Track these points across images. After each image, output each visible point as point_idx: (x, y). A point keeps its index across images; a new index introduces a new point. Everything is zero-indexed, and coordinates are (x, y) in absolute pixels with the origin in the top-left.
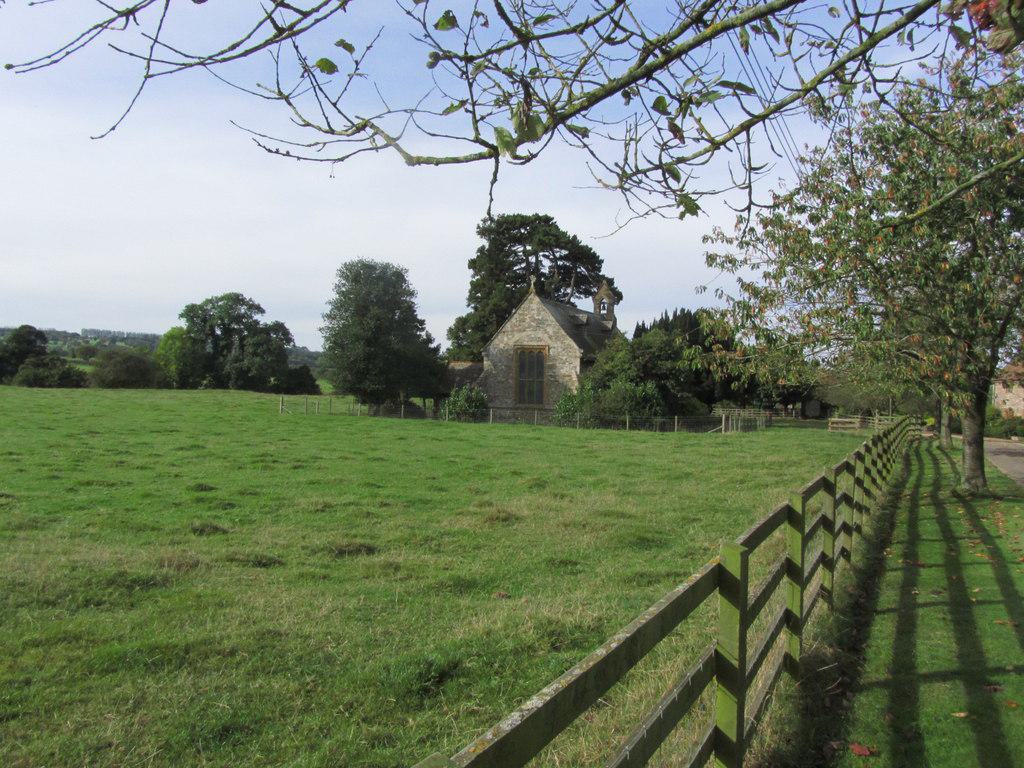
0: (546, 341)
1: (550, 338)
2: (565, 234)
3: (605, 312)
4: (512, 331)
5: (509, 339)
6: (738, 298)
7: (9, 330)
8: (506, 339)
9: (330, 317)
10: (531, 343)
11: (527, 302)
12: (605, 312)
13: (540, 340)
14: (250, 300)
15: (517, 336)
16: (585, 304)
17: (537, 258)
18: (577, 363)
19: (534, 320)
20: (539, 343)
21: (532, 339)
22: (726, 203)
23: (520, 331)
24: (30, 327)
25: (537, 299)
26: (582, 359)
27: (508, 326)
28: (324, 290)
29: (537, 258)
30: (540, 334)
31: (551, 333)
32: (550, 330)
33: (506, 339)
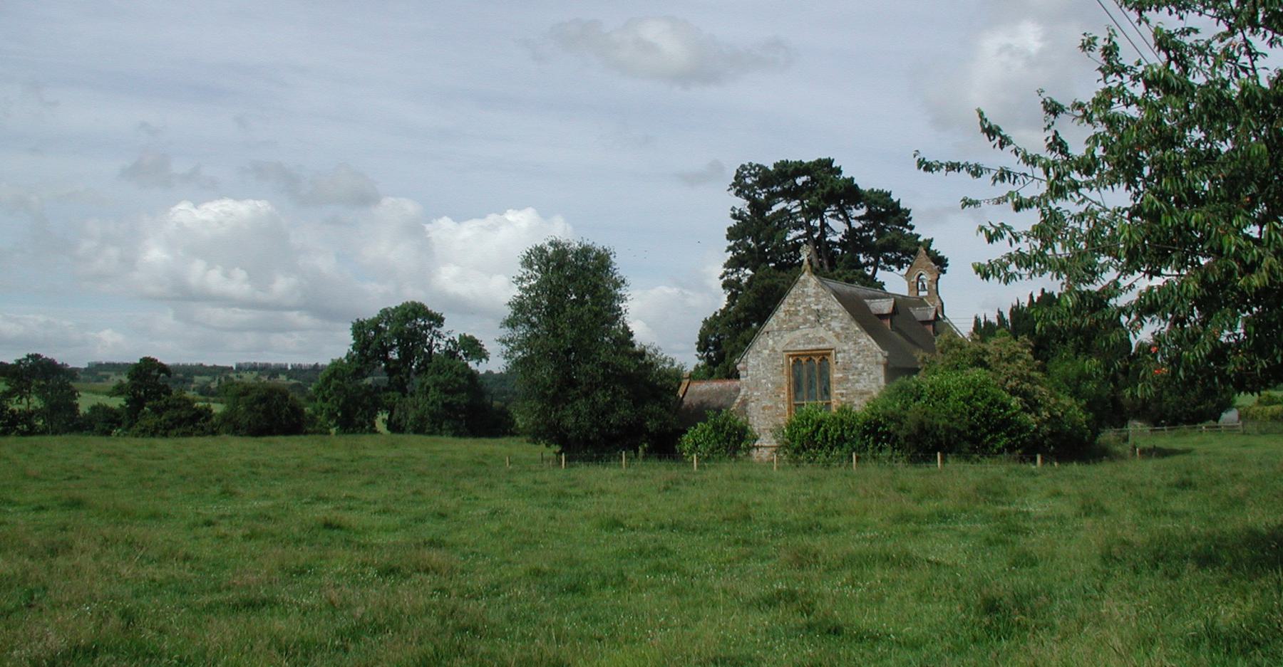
0: (831, 341)
1: (837, 335)
2: (374, 319)
3: (925, 293)
4: (780, 330)
5: (775, 342)
6: (518, 295)
7: (126, 365)
8: (771, 342)
9: (511, 323)
10: (810, 347)
11: (799, 285)
12: (925, 293)
13: (823, 340)
14: (1097, 93)
15: (788, 337)
16: (894, 281)
17: (822, 221)
18: (880, 373)
19: (811, 312)
20: (821, 346)
21: (809, 342)
22: (928, 167)
23: (792, 329)
24: (153, 360)
25: (813, 280)
26: (886, 366)
27: (772, 323)
28: (913, 224)
29: (822, 221)
30: (821, 332)
31: (838, 329)
32: (836, 325)
33: (771, 342)
